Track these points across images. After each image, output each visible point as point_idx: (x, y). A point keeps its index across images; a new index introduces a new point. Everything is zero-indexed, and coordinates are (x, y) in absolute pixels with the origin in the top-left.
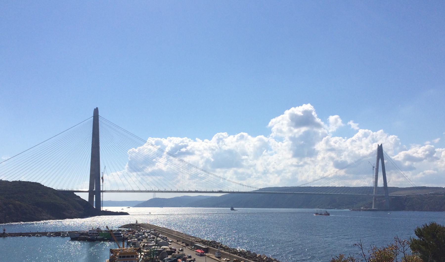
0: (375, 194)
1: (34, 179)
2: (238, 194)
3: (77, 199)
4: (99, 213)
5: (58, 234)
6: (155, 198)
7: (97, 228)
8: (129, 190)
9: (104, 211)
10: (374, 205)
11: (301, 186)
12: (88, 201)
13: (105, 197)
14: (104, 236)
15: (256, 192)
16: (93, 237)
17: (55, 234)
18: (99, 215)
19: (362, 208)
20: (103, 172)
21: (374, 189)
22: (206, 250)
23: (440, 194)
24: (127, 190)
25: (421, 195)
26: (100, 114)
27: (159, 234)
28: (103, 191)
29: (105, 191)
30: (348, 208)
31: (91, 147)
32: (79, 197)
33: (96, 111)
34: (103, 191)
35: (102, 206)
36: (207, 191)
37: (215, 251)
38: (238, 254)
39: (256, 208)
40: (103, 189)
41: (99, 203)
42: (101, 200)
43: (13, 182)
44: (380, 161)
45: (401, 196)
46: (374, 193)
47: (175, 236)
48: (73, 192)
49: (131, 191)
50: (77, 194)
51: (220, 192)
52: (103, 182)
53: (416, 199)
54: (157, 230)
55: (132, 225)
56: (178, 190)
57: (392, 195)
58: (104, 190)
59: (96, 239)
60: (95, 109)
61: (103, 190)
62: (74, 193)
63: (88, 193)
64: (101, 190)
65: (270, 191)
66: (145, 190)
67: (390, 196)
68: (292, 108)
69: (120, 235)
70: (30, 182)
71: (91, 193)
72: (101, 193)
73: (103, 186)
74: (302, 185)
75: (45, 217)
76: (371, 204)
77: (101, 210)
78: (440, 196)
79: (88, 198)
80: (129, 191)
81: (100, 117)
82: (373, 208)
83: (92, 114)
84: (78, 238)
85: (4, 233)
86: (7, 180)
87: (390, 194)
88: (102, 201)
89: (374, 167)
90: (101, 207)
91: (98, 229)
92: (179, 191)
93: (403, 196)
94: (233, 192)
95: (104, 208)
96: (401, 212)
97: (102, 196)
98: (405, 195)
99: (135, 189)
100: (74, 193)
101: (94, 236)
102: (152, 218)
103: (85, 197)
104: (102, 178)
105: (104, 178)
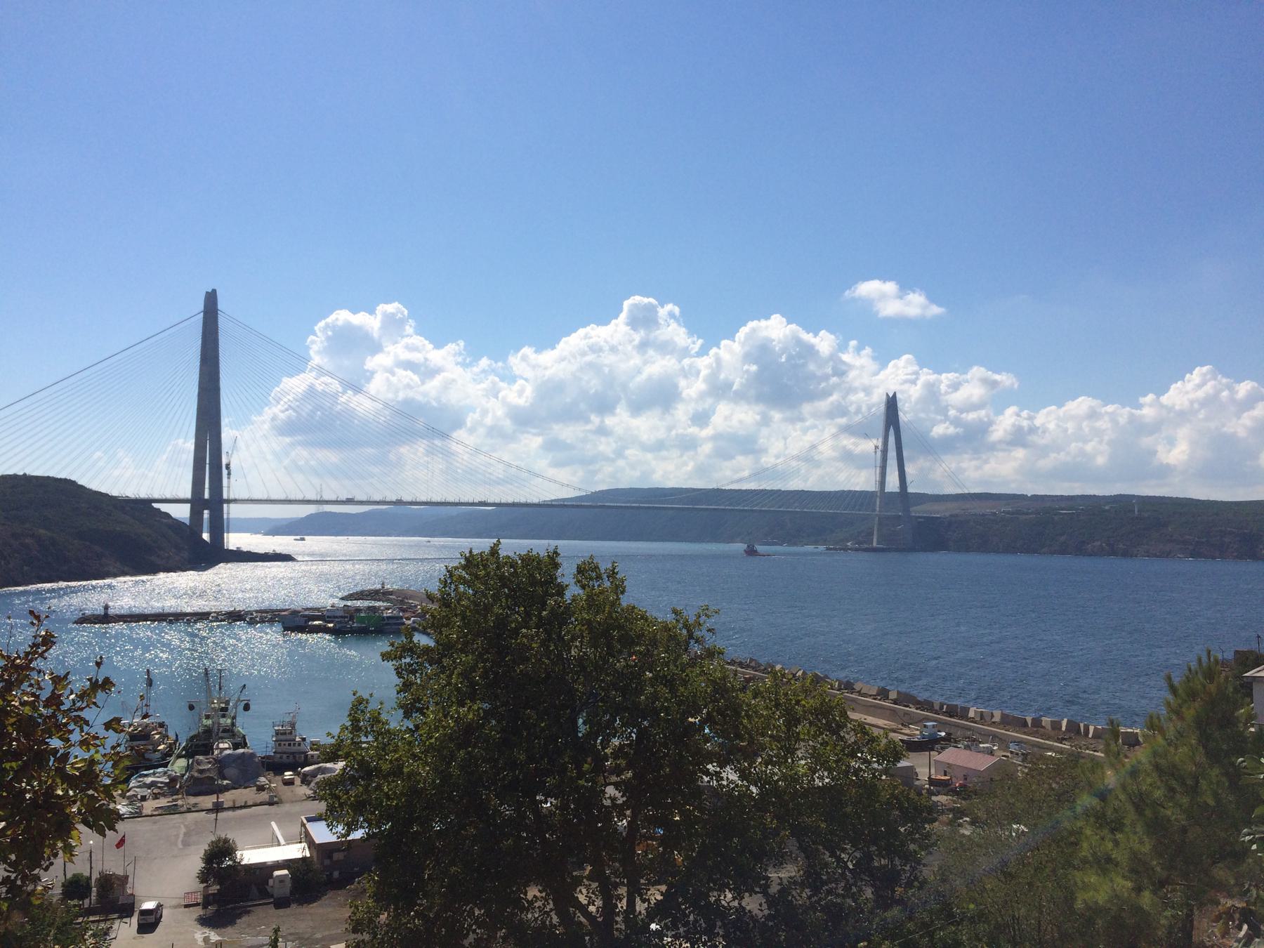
0: (880, 511)
13: (232, 512)
18: (227, 561)
19: (849, 544)
26: (220, 306)
28: (229, 501)
29: (235, 501)
30: (816, 543)
32: (167, 515)
33: (211, 301)
34: (229, 501)
35: (228, 532)
40: (228, 496)
41: (218, 528)
42: (225, 516)
44: (892, 432)
46: (878, 509)
50: (164, 508)
52: (229, 478)
57: (917, 515)
58: (232, 497)
60: (207, 292)
62: (153, 504)
63: (189, 505)
64: (225, 496)
71: (197, 502)
72: (225, 506)
73: (229, 487)
80: (296, 501)
81: (222, 314)
83: (200, 305)
88: (228, 519)
90: (225, 534)
92: (340, 501)
95: (234, 541)
98: (947, 514)
100: (153, 504)
103: (182, 512)
104: (228, 467)
105: (232, 466)
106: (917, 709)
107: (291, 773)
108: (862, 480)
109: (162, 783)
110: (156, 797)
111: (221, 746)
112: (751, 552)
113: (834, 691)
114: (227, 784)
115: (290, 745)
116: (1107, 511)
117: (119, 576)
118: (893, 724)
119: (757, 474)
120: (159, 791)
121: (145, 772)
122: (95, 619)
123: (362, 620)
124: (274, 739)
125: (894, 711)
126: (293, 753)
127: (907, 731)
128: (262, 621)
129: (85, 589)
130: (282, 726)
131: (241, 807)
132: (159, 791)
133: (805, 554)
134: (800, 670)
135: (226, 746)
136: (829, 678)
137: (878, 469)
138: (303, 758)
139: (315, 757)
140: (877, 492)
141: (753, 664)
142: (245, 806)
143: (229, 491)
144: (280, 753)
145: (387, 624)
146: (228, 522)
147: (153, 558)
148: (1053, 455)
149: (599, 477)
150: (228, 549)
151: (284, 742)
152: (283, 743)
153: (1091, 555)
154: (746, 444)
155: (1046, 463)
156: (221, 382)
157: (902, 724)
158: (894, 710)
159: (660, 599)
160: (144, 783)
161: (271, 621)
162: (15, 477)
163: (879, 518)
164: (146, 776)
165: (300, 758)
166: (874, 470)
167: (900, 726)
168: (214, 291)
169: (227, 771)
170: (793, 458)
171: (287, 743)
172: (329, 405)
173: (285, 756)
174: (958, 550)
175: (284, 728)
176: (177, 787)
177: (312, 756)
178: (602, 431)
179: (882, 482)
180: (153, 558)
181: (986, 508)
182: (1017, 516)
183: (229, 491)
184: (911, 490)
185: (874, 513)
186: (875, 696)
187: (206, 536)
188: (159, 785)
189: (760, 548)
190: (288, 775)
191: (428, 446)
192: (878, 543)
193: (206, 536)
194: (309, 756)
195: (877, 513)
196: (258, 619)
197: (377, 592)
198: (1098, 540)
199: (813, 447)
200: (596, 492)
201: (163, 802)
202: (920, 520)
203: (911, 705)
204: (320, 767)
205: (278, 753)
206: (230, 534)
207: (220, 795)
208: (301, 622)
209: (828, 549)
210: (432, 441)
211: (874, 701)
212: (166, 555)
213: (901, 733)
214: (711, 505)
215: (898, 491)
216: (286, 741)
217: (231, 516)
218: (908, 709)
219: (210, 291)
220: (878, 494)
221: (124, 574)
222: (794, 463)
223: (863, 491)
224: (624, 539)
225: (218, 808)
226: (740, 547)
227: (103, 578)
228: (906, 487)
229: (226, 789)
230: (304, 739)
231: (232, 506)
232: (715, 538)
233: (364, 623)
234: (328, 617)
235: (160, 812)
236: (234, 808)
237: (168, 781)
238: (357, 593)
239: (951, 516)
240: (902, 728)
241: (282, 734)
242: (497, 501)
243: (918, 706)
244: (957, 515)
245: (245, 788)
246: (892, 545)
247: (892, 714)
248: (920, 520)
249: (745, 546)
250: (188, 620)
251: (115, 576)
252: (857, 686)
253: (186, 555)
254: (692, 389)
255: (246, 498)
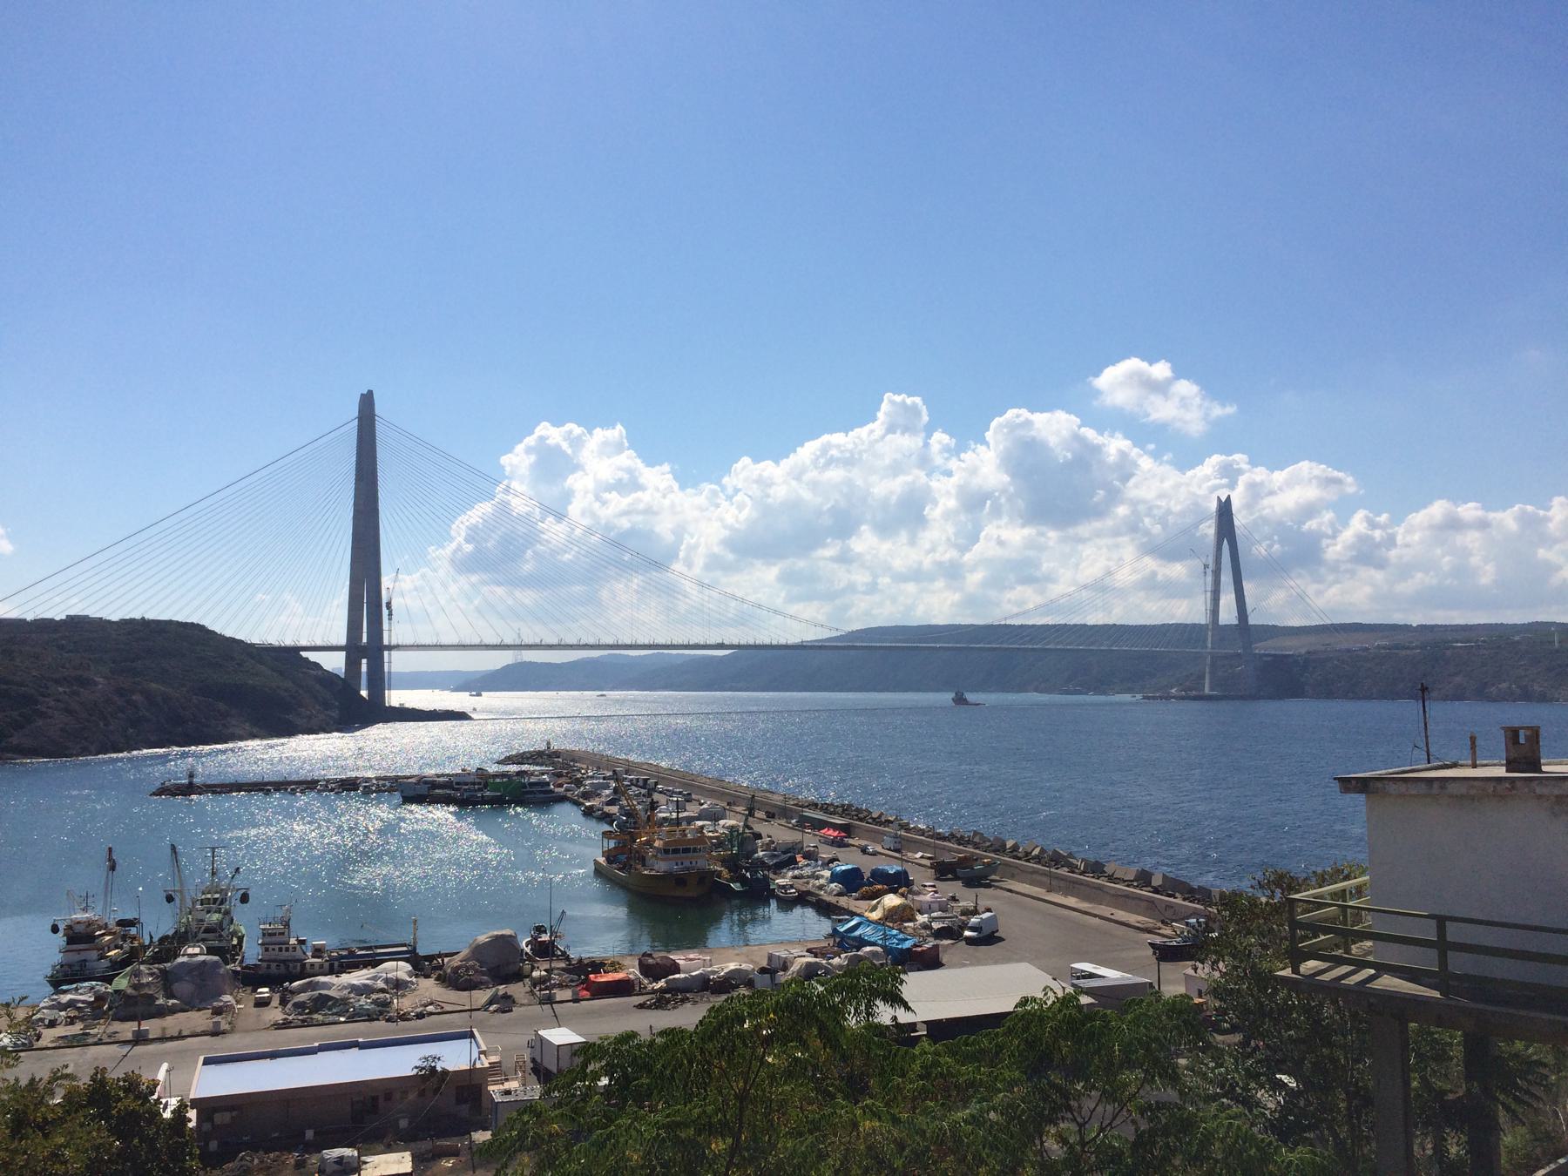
0: (1212, 648)
1: (114, 612)
2: (775, 652)
3: (315, 673)
4: (377, 712)
5: (350, 785)
6: (519, 663)
7: (478, 769)
8: (469, 644)
9: (395, 708)
10: (1211, 683)
11: (1017, 622)
12: (343, 676)
13: (396, 663)
14: (502, 790)
15: (824, 644)
16: (471, 793)
17: (342, 785)
18: (386, 721)
19: (1173, 691)
20: (391, 587)
21: (1210, 633)
22: (847, 830)
23: (1408, 648)
24: (442, 644)
25: (1348, 651)
26: (378, 411)
27: (656, 784)
28: (390, 648)
29: (397, 647)
30: (1129, 690)
31: (352, 515)
32: (317, 666)
33: (367, 401)
34: (390, 648)
35: (389, 689)
36: (708, 643)
37: (884, 833)
38: (1313, 881)
39: (841, 691)
40: (390, 641)
41: (378, 681)
42: (386, 670)
43: (125, 623)
45: (1291, 653)
46: (1210, 645)
47: (713, 791)
48: (295, 651)
49: (475, 646)
50: (312, 656)
51: (721, 646)
52: (390, 619)
53: (1335, 662)
54: (634, 771)
55: (534, 755)
56: (620, 643)
57: (1263, 652)
58: (394, 642)
59: (480, 799)
60: (362, 395)
61: (392, 644)
62: (301, 653)
64: (386, 642)
65: (899, 641)
66: (519, 643)
67: (1259, 654)
68: (1108, 366)
69: (546, 788)
70: (178, 624)
71: (353, 650)
72: (386, 653)
73: (390, 630)
74: (1006, 619)
75: (238, 731)
76: (1202, 677)
77: (387, 705)
78: (1408, 652)
79: (442, 670)
81: (381, 420)
82: (1207, 691)
83: (354, 411)
84: (427, 797)
85: (191, 783)
86: (21, 617)
87: (1261, 648)
88: (389, 673)
89: (1206, 566)
90: (386, 692)
91: (480, 772)
92: (504, 646)
93: (1297, 652)
94: (786, 647)
95: (396, 698)
96: (1282, 702)
97: (390, 662)
98: (1303, 651)
99: (508, 641)
100: (301, 653)
101: (476, 791)
102: (559, 726)
103: (334, 663)
104: (389, 605)
106: (1184, 899)
107: (266, 990)
108: (1188, 610)
109: (83, 1002)
110: (71, 1021)
111: (190, 951)
112: (960, 700)
113: (1075, 875)
114: (173, 1004)
115: (280, 950)
116: (1518, 642)
117: (247, 739)
118: (1151, 921)
119: (1047, 608)
120: (77, 1013)
121: (64, 987)
122: (176, 789)
123: (496, 787)
124: (260, 942)
125: (1153, 902)
126: (284, 961)
127: (1168, 931)
128: (378, 791)
129: (224, 752)
130: (270, 924)
131: (172, 1039)
132: (77, 1013)
133: (1120, 704)
134: (1037, 846)
135: (197, 950)
136: (1074, 858)
137: (1209, 594)
138: (299, 968)
139: (317, 967)
140: (1207, 625)
141: (977, 839)
142: (180, 1037)
143: (390, 636)
144: (269, 961)
145: (528, 793)
146: (390, 679)
147: (290, 717)
148: (1419, 575)
149: (851, 613)
150: (390, 706)
151: (273, 947)
152: (271, 947)
153: (1495, 701)
154: (1024, 571)
155: (1406, 587)
156: (380, 504)
157: (1163, 922)
158: (1151, 901)
159: (572, 764)
160: (59, 1003)
161: (391, 790)
162: (132, 621)
163: (1212, 658)
164: (65, 992)
165: (295, 967)
166: (1204, 596)
167: (1159, 924)
168: (370, 393)
169: (176, 987)
170: (1085, 587)
171: (277, 947)
172: (524, 530)
173: (273, 965)
174: (1318, 696)
175: (272, 927)
176: (105, 1008)
177: (312, 965)
178: (845, 558)
179: (1215, 611)
180: (290, 717)
181: (1344, 642)
182: (1396, 651)
183: (390, 636)
184: (1252, 621)
185: (1204, 651)
186: (1132, 881)
187: (364, 693)
188: (80, 1005)
189: (970, 697)
190: (264, 991)
191: (642, 581)
192: (1212, 689)
193: (364, 693)
194: (308, 966)
195: (1209, 650)
196: (374, 788)
197: (540, 754)
198: (1505, 681)
199: (1109, 573)
200: (853, 632)
201: (77, 1028)
202: (1265, 659)
203: (1177, 895)
204: (312, 981)
205: (265, 961)
206: (392, 691)
207: (142, 1022)
208: (423, 790)
209: (1144, 698)
210: (648, 575)
211: (1127, 888)
212: (308, 712)
213: (1159, 934)
214: (979, 643)
215: (1237, 622)
216: (275, 944)
217: (393, 670)
218: (1172, 899)
219: (365, 392)
220: (1210, 627)
221: (253, 736)
222: (1084, 593)
223: (1180, 624)
224: (888, 690)
225: (140, 1039)
226: (950, 696)
227: (226, 742)
228: (1247, 617)
229: (172, 1011)
230: (302, 942)
231: (394, 653)
232: (1005, 688)
233: (500, 792)
234: (458, 784)
235: (61, 1043)
236: (162, 1039)
237: (92, 999)
238: (516, 756)
239: (1309, 653)
240: (1161, 926)
241: (270, 935)
242: (735, 642)
243: (1187, 896)
244: (1315, 652)
245: (199, 1010)
246: (1229, 691)
247: (1150, 907)
248: (1265, 659)
249: (952, 695)
250: (291, 789)
251: (242, 739)
252: (1109, 869)
253: (335, 714)
254: (945, 496)
255: (412, 644)
